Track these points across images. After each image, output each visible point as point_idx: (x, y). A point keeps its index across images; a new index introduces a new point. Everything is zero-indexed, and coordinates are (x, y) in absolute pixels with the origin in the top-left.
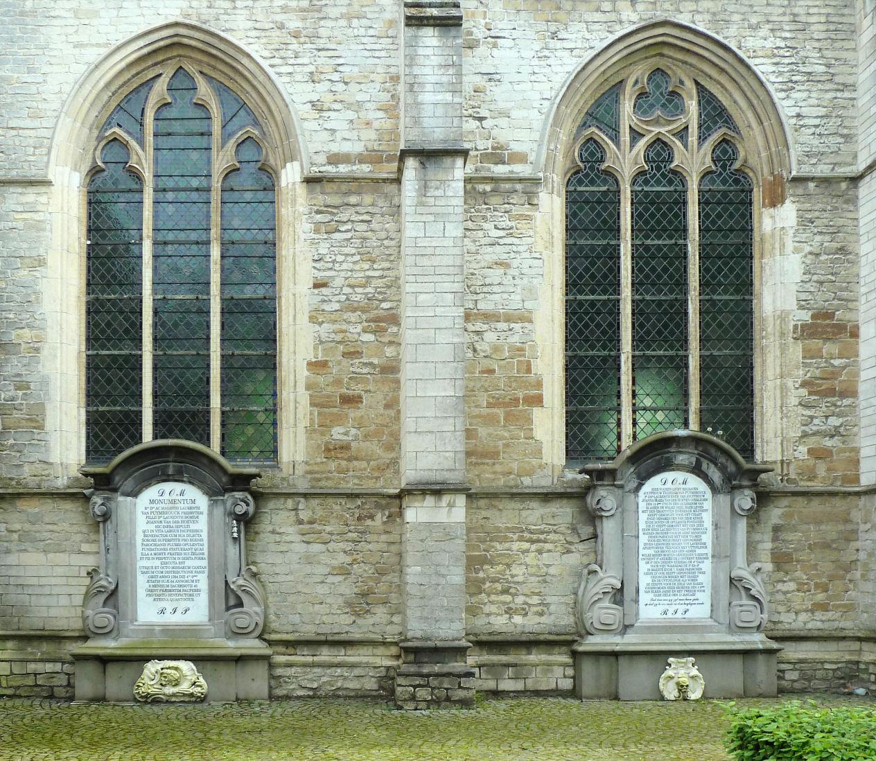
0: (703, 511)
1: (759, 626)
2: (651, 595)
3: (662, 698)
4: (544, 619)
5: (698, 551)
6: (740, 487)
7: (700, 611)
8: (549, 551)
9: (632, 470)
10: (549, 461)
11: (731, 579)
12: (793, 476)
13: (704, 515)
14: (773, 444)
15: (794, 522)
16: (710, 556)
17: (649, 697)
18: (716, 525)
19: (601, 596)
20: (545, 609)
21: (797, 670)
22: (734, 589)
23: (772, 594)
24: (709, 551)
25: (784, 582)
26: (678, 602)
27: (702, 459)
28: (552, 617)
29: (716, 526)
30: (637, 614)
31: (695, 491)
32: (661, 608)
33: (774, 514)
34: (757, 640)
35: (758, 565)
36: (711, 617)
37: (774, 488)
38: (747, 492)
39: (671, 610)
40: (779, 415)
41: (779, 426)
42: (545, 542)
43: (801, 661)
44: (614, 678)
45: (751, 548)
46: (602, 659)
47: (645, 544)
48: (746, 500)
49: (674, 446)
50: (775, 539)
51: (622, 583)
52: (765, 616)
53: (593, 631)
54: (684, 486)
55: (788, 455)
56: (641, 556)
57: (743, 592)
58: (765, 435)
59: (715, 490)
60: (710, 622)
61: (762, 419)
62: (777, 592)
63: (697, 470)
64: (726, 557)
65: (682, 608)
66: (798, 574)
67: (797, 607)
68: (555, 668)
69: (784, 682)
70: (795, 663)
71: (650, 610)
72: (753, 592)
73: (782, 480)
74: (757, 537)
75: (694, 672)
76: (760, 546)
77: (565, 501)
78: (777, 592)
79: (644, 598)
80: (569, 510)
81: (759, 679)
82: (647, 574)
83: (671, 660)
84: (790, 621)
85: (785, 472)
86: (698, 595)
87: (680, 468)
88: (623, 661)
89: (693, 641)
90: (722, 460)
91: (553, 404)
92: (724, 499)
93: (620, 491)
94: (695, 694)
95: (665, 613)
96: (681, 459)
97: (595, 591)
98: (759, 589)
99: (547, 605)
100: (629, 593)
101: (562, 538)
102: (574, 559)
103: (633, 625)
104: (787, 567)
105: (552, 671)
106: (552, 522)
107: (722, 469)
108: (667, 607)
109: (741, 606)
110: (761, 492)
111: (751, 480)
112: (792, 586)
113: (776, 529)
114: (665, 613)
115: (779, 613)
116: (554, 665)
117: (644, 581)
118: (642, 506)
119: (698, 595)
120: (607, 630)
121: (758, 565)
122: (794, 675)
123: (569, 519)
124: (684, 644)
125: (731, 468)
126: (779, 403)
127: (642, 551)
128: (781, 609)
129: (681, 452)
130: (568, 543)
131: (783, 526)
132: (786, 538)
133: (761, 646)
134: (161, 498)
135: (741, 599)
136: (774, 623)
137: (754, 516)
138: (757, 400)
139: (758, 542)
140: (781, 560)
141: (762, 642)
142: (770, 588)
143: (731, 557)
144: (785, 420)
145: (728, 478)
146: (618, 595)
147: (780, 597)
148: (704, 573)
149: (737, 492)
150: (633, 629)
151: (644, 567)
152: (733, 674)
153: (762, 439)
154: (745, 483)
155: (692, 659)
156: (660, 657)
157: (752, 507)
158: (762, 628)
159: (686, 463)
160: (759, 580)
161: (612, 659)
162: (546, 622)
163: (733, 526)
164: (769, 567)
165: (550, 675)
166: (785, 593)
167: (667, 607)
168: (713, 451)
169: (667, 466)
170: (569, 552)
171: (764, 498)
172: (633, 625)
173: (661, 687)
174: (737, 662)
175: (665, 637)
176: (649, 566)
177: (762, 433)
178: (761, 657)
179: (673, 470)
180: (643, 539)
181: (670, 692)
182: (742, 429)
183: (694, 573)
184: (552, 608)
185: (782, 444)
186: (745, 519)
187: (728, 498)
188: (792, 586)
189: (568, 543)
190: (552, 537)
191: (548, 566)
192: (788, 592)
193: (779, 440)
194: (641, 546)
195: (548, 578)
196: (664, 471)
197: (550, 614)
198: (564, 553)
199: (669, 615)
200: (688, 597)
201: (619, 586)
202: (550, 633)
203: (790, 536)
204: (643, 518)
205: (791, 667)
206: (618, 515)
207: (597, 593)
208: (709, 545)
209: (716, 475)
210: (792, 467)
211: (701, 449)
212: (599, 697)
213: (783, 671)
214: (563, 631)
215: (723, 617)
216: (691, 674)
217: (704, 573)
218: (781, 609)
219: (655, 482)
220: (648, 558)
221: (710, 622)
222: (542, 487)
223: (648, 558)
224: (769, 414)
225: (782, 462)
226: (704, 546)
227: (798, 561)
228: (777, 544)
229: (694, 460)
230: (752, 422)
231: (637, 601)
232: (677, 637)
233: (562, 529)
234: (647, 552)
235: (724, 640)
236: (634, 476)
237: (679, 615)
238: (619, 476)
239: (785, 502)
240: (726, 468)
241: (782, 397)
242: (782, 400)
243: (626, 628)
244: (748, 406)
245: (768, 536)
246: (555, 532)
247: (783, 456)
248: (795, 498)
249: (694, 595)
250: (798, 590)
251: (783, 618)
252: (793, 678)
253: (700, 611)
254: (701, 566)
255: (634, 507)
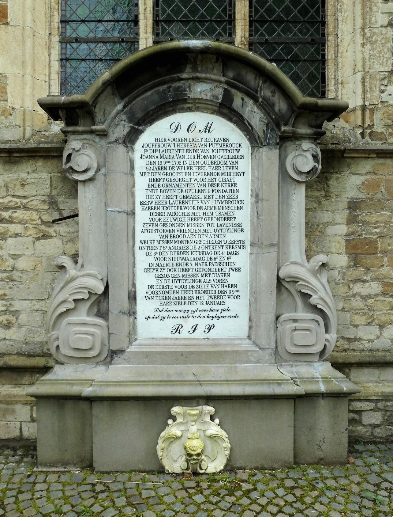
0: (237, 174)
1: (322, 353)
2: (155, 304)
3: (161, 471)
4: (11, 334)
5: (230, 236)
6: (295, 137)
7: (232, 328)
8: (17, 235)
9: (119, 107)
10: (18, 104)
11: (279, 280)
12: (379, 128)
13: (239, 180)
14: (351, 85)
15: (379, 196)
16: (247, 244)
17: (141, 467)
18: (257, 196)
19: (72, 306)
20: (13, 319)
21: (379, 409)
22: (285, 295)
23: (346, 299)
24: (246, 236)
25: (364, 281)
26: (197, 314)
27: (234, 91)
28: (23, 330)
29: (257, 197)
30: (132, 334)
31: (224, 143)
32: (171, 323)
33: (351, 183)
34: (319, 375)
35: (321, 258)
36: (249, 337)
37: (352, 146)
38: (306, 145)
39: (188, 325)
40: (359, 40)
41: (359, 56)
42: (11, 221)
43: (386, 398)
44: (85, 437)
45: (314, 232)
46: (69, 405)
47: (145, 225)
48: (304, 158)
49: (188, 69)
50: (351, 220)
51: (107, 287)
52: (332, 336)
53: (62, 359)
54: (207, 135)
55: (373, 98)
56: (138, 244)
57: (299, 300)
58: (340, 74)
59: (255, 141)
60: (247, 345)
61: (336, 53)
62: (354, 296)
63: (225, 109)
64: (272, 245)
65: (203, 324)
66: (384, 271)
67: (383, 318)
68: (18, 407)
69: (360, 428)
70: (378, 401)
71: (153, 326)
72: (314, 300)
73: (363, 135)
74: (325, 216)
75: (214, 429)
76: (330, 230)
77: (40, 163)
78: (354, 296)
79: (144, 307)
80: (44, 175)
81: (320, 435)
82: (148, 271)
83: (176, 410)
84: (372, 337)
85: (368, 122)
86: (229, 303)
87: (198, 105)
88: (98, 410)
89: (218, 379)
90: (266, 92)
91: (24, 21)
92: (270, 155)
93: (103, 142)
94: (214, 465)
95: (178, 330)
96: (200, 90)
97: (60, 298)
98: (322, 293)
99: (15, 313)
100: (118, 300)
101: (35, 216)
102: (51, 247)
103: (122, 351)
104: (368, 260)
105: (14, 411)
106: (21, 193)
107: (266, 106)
108: (181, 321)
109: (295, 321)
110: (332, 151)
111: (311, 126)
112: (375, 287)
113: (354, 206)
114: (178, 330)
115: (356, 326)
116: (17, 403)
117: (144, 281)
118: (140, 165)
119: (229, 303)
120: (82, 358)
121: (321, 258)
122: (376, 418)
123: (46, 190)
124: (200, 383)
125: (281, 105)
126: (359, 22)
127: (140, 237)
128: (359, 320)
129: (198, 80)
130: (44, 223)
131: (363, 200)
132: (367, 218)
133: (322, 388)
134: (174, 136)
135: (295, 310)
136: (349, 340)
137: (319, 182)
138: (330, 28)
139: (327, 224)
140: (359, 251)
141: (326, 380)
142: (342, 290)
143: (279, 245)
144: (368, 47)
145: (275, 121)
146: (100, 303)
147: (357, 303)
148: (239, 270)
149: (291, 146)
150: (125, 355)
151: (143, 260)
152: (276, 434)
153: (336, 80)
154: (303, 130)
155: (210, 409)
156: (158, 406)
157: (314, 170)
158: (327, 356)
159: (209, 97)
160: (325, 281)
161: (84, 405)
162: (14, 337)
163: (284, 200)
164: (343, 260)
165: (10, 418)
166: (365, 298)
167: (181, 321)
168: (251, 78)
169: (176, 103)
170: (45, 236)
171: (334, 159)
172: (122, 351)
173: (160, 454)
174: (284, 415)
175: (172, 370)
176: (151, 259)
177: (336, 71)
178: (322, 402)
179: (189, 110)
180: (142, 217)
181: (175, 463)
182: (312, 62)
183: (228, 266)
184: (23, 317)
185: (363, 82)
186: (303, 188)
187: (274, 153)
188: (375, 287)
189: (44, 223)
190: (20, 214)
191: (15, 257)
192: (369, 296)
193: (359, 76)
194: (139, 228)
195: (16, 275)
196: (175, 111)
197: (20, 326)
198: (38, 239)
199: (185, 333)
200: (214, 307)
201: (101, 289)
202: (19, 354)
203: (374, 217)
204: (141, 184)
205: (371, 406)
206: (100, 178)
207: (65, 301)
208: (247, 226)
209: (256, 117)
210: (378, 116)
211: (231, 74)
212: (65, 464)
213: (359, 412)
214: (38, 350)
215: (266, 338)
216: (210, 432)
217: (239, 270)
218: (359, 320)
219: (161, 128)
220: (149, 247)
221: (247, 345)
222: (7, 142)
223: (149, 247)
224: (345, 43)
225: (364, 108)
226: (238, 227)
227: (384, 252)
228: (353, 227)
229: (219, 92)
230: (323, 61)
231: (132, 313)
232: (189, 371)
233: (36, 203)
234: (148, 237)
235: (265, 375)
236: (124, 117)
237: (199, 333)
238: (99, 116)
239: (367, 166)
240: (272, 105)
241: (364, 15)
242: (364, 19)
243: (112, 355)
244: (318, 37)
245: (342, 215)
246: (25, 207)
247: (364, 99)
248: (381, 161)
249: (223, 303)
250: (384, 294)
251: (360, 333)
252: (373, 421)
253: (232, 328)
254: (234, 259)
255: (124, 167)
